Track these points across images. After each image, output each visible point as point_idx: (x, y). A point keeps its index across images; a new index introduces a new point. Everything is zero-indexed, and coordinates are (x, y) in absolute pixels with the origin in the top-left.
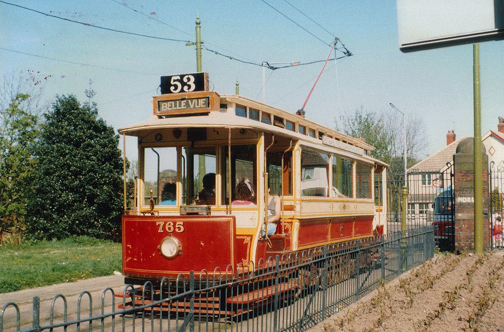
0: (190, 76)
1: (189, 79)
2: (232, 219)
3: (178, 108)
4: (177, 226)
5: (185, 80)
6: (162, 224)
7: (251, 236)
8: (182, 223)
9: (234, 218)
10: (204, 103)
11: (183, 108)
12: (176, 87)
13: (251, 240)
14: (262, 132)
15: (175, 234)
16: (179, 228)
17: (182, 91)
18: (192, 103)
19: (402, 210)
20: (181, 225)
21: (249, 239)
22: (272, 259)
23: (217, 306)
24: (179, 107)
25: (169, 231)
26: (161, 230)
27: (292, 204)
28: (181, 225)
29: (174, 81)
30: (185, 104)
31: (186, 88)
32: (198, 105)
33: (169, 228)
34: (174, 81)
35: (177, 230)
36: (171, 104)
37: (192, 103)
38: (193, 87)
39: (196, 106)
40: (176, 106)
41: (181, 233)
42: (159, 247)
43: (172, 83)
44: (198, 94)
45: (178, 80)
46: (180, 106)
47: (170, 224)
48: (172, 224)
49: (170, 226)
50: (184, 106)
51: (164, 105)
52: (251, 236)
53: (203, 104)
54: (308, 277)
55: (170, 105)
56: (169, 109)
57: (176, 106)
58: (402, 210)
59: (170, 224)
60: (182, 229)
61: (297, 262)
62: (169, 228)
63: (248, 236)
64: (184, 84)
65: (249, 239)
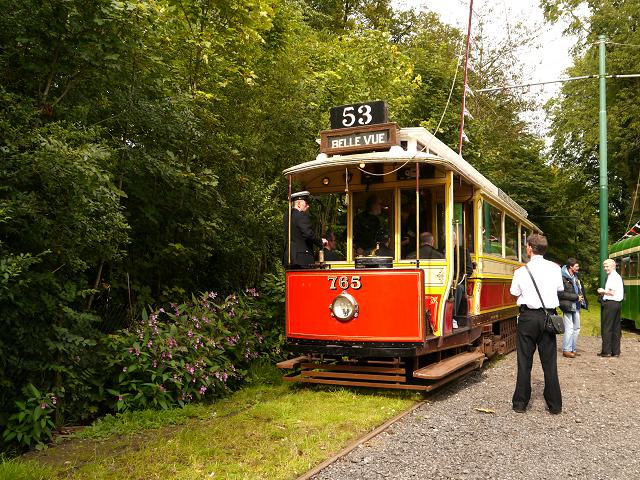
1: (365, 110)
5: (360, 111)
7: (439, 296)
8: (358, 277)
9: (422, 271)
12: (349, 120)
16: (355, 284)
17: (356, 123)
22: (89, 210)
23: (403, 379)
24: (404, 256)
31: (361, 121)
34: (347, 112)
35: (352, 286)
40: (348, 143)
45: (351, 112)
46: (353, 143)
52: (439, 296)
57: (348, 143)
63: (434, 296)
64: (358, 116)
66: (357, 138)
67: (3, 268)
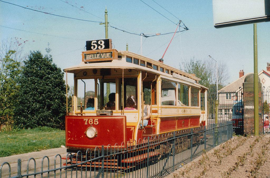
0: (102, 41)
1: (101, 43)
2: (124, 117)
3: (95, 58)
4: (95, 121)
5: (99, 43)
6: (87, 120)
7: (135, 127)
8: (97, 120)
9: (125, 117)
10: (109, 55)
11: (98, 58)
12: (94, 47)
13: (134, 129)
14: (140, 71)
15: (94, 125)
16: (96, 122)
17: (98, 49)
18: (103, 55)
19: (215, 113)
20: (97, 120)
21: (133, 128)
22: (145, 139)
23: (117, 164)
24: (96, 57)
25: (91, 124)
26: (86, 124)
27: (156, 109)
28: (97, 120)
29: (93, 43)
30: (99, 56)
31: (99, 47)
32: (106, 56)
33: (91, 123)
34: (93, 43)
35: (95, 123)
36: (92, 56)
37: (103, 55)
38: (104, 46)
39: (105, 57)
40: (94, 57)
41: (97, 125)
42: (85, 132)
43: (92, 44)
44: (106, 50)
45: (95, 43)
46: (96, 57)
47: (91, 120)
48: (92, 120)
49: (91, 121)
50: (99, 57)
51: (88, 56)
52: (135, 127)
53: (109, 56)
54: (165, 149)
55: (91, 57)
56: (90, 58)
57: (94, 57)
58: (215, 113)
59: (91, 120)
60: (98, 123)
61: (159, 140)
62: (91, 123)
63: (133, 126)
64: (98, 45)
65: (133, 128)
66: (98, 54)
67: (211, 177)
